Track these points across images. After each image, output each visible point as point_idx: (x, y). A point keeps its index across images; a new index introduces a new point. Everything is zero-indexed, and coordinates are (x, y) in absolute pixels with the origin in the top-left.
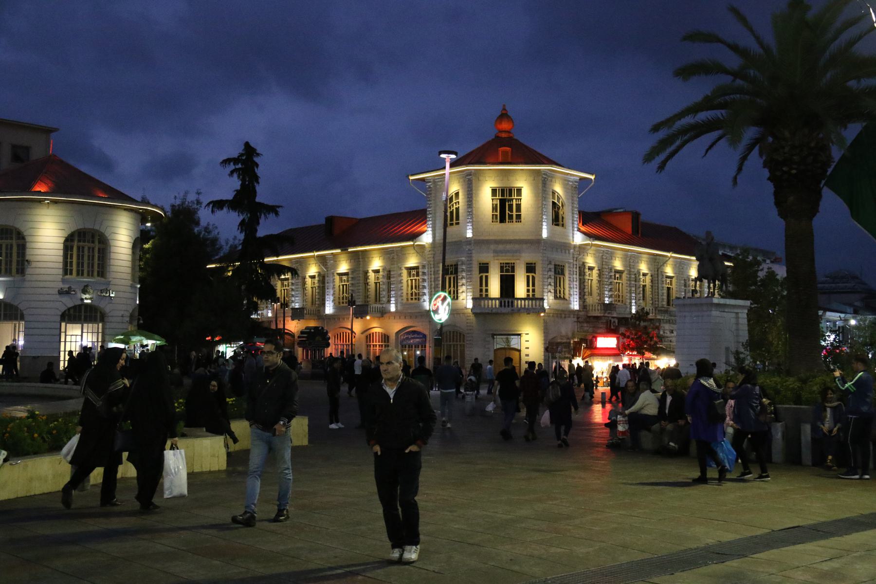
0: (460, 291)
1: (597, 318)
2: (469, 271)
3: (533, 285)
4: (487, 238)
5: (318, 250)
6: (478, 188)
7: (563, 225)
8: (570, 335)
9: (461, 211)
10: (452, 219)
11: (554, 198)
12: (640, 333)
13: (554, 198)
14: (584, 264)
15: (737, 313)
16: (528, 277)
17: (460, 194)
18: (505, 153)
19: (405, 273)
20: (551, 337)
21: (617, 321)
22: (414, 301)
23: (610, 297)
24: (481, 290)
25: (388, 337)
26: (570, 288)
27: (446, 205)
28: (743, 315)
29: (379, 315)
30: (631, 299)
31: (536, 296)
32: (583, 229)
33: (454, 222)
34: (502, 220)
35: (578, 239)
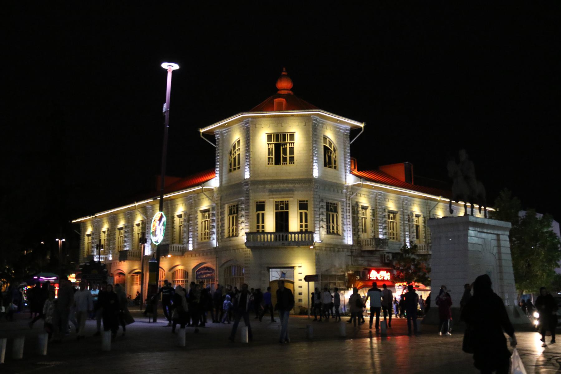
0: (240, 228)
1: (371, 252)
2: (247, 209)
3: (306, 221)
4: (262, 179)
5: (137, 201)
6: (255, 135)
7: (335, 168)
8: (344, 267)
9: (241, 156)
10: (235, 165)
11: (325, 142)
12: (407, 265)
13: (325, 142)
14: (357, 204)
15: (498, 235)
16: (301, 214)
17: (241, 141)
18: (280, 104)
19: (200, 215)
20: (324, 269)
21: (391, 255)
22: (206, 240)
23: (385, 234)
24: (258, 227)
25: (188, 273)
26: (343, 224)
27: (231, 153)
28: (505, 238)
29: (180, 253)
30: (405, 237)
31: (309, 230)
32: (355, 172)
33: (237, 166)
34: (277, 162)
35: (350, 180)
